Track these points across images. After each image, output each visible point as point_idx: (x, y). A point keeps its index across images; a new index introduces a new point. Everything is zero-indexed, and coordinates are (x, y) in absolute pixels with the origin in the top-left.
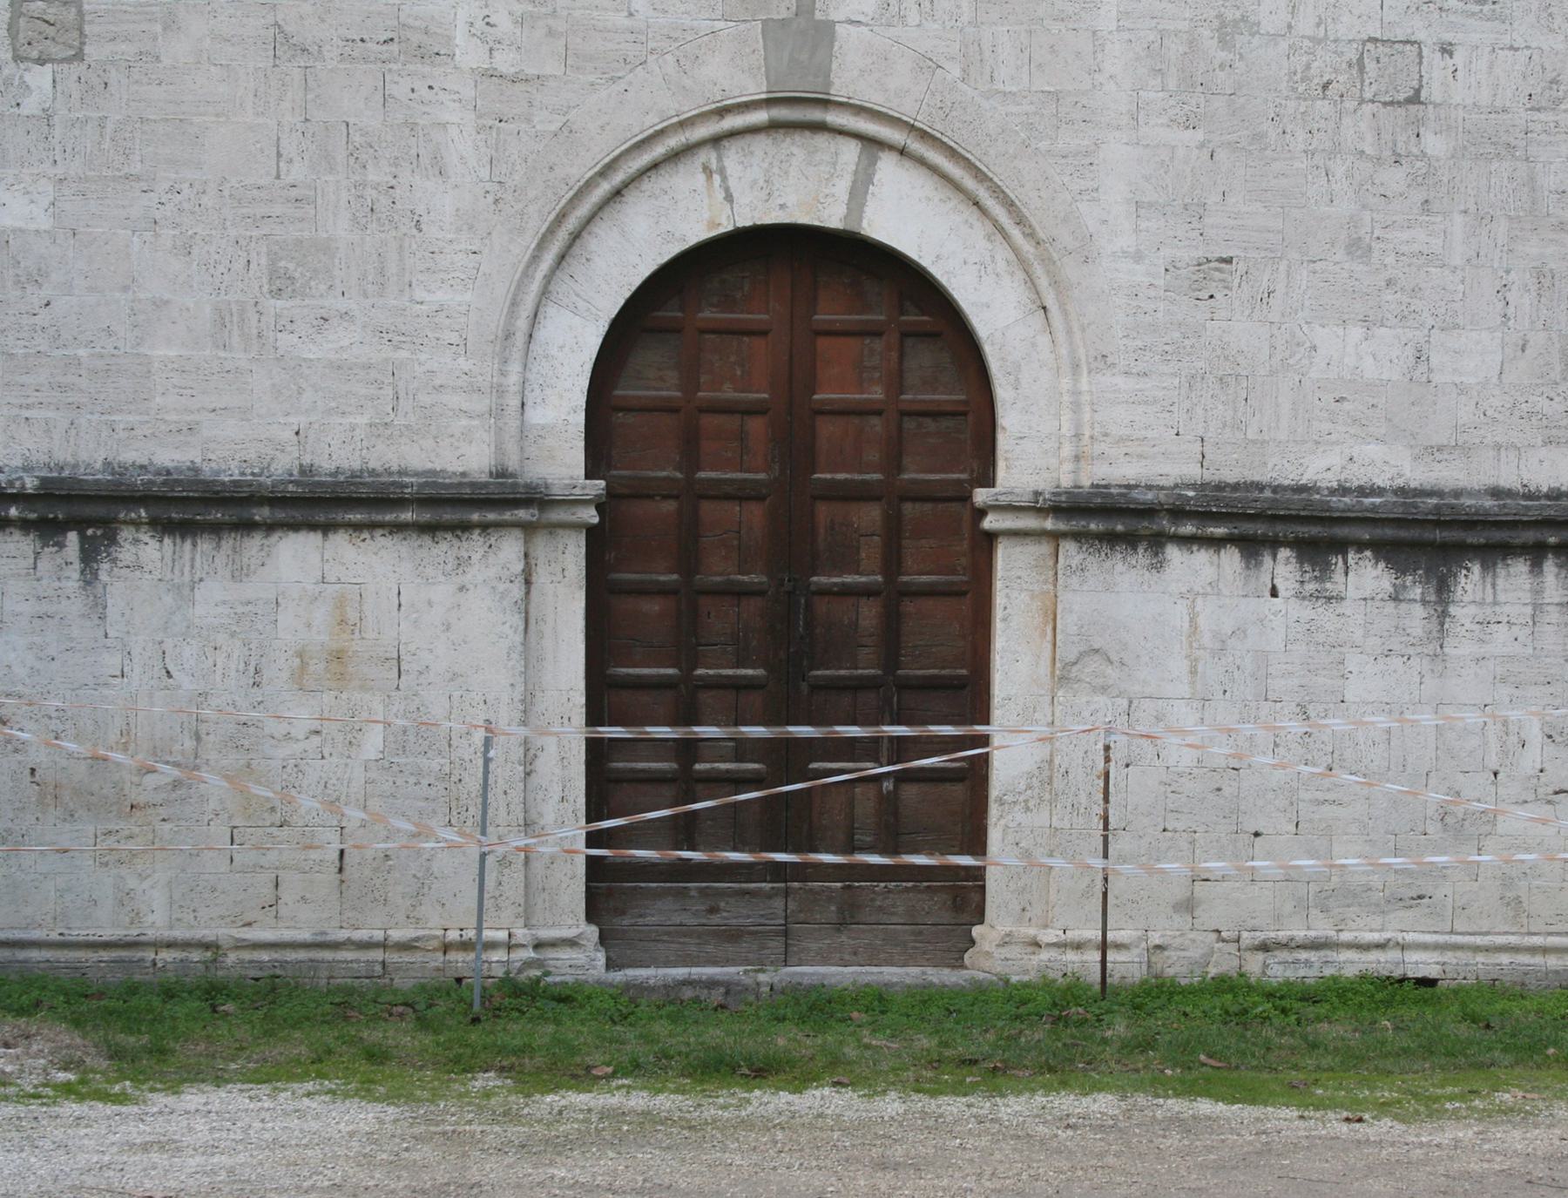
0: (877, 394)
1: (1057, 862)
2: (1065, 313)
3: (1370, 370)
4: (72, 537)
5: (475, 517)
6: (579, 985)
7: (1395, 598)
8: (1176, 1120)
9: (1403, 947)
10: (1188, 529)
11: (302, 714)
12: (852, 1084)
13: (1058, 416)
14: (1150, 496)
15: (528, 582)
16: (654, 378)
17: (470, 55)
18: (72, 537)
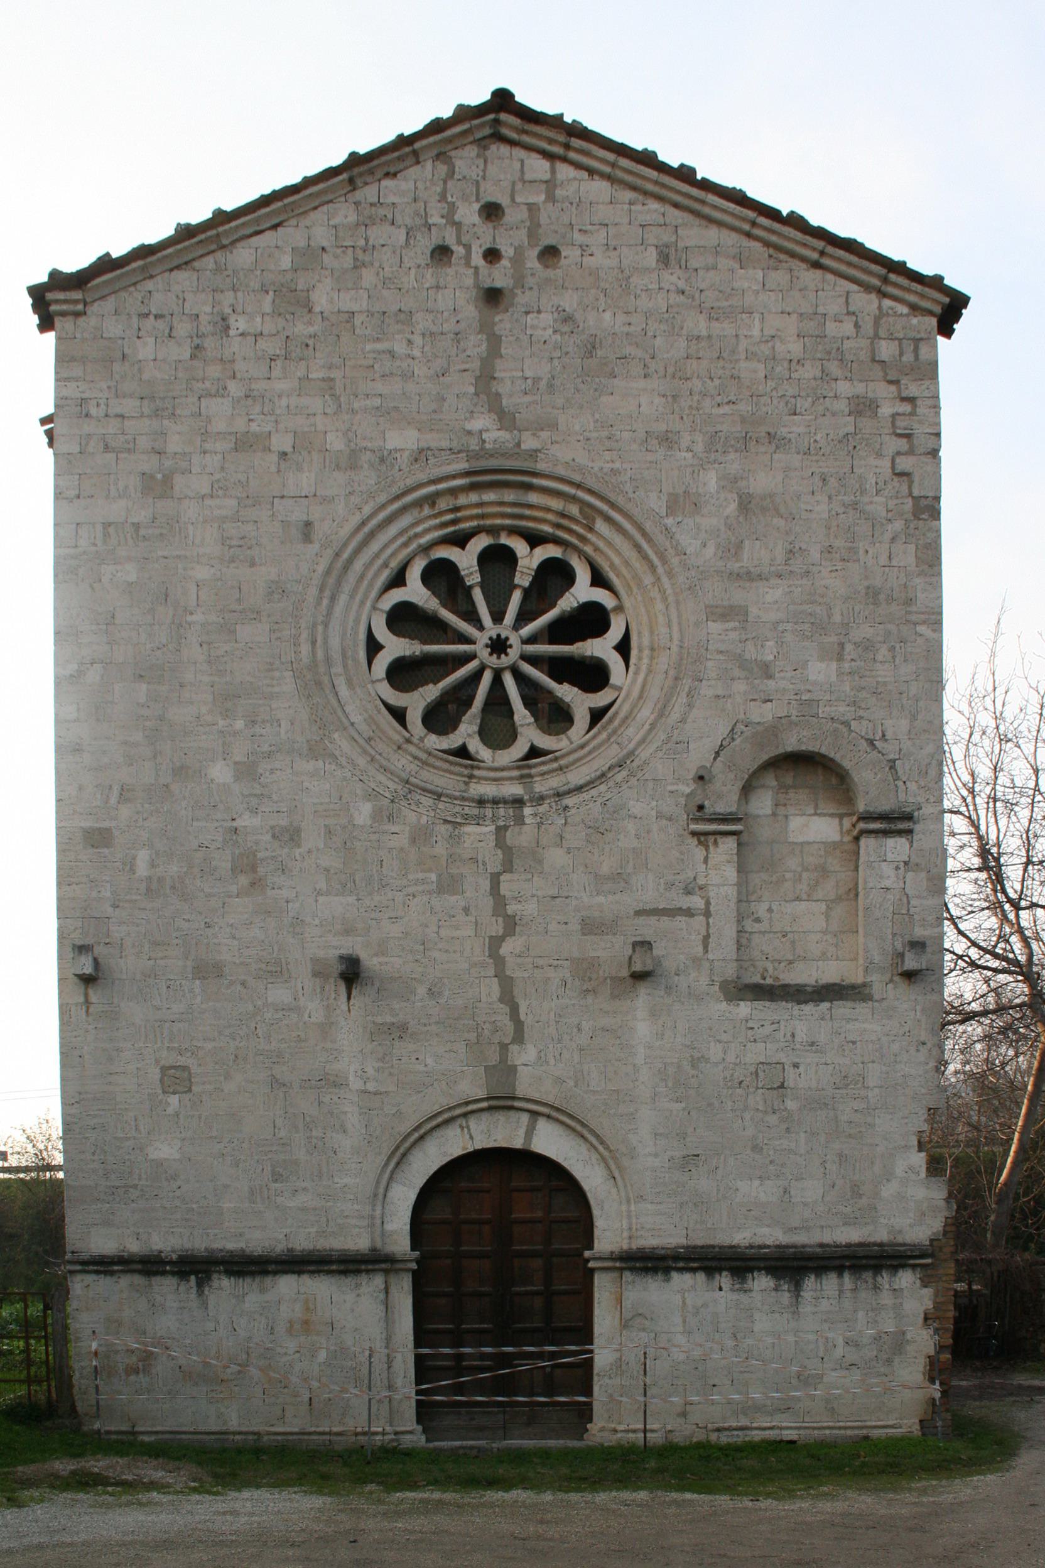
0: (539, 1214)
1: (624, 1399)
2: (623, 1179)
3: (763, 1197)
4: (193, 1278)
5: (363, 1267)
6: (413, 1449)
7: (776, 1289)
8: (675, 1502)
9: (781, 1428)
10: (681, 1264)
11: (291, 1345)
12: (532, 1489)
13: (621, 1221)
14: (663, 1252)
15: (387, 1292)
16: (441, 1210)
17: (355, 1084)
18: (193, 1278)
